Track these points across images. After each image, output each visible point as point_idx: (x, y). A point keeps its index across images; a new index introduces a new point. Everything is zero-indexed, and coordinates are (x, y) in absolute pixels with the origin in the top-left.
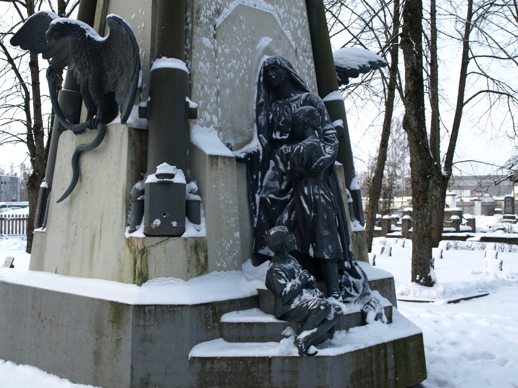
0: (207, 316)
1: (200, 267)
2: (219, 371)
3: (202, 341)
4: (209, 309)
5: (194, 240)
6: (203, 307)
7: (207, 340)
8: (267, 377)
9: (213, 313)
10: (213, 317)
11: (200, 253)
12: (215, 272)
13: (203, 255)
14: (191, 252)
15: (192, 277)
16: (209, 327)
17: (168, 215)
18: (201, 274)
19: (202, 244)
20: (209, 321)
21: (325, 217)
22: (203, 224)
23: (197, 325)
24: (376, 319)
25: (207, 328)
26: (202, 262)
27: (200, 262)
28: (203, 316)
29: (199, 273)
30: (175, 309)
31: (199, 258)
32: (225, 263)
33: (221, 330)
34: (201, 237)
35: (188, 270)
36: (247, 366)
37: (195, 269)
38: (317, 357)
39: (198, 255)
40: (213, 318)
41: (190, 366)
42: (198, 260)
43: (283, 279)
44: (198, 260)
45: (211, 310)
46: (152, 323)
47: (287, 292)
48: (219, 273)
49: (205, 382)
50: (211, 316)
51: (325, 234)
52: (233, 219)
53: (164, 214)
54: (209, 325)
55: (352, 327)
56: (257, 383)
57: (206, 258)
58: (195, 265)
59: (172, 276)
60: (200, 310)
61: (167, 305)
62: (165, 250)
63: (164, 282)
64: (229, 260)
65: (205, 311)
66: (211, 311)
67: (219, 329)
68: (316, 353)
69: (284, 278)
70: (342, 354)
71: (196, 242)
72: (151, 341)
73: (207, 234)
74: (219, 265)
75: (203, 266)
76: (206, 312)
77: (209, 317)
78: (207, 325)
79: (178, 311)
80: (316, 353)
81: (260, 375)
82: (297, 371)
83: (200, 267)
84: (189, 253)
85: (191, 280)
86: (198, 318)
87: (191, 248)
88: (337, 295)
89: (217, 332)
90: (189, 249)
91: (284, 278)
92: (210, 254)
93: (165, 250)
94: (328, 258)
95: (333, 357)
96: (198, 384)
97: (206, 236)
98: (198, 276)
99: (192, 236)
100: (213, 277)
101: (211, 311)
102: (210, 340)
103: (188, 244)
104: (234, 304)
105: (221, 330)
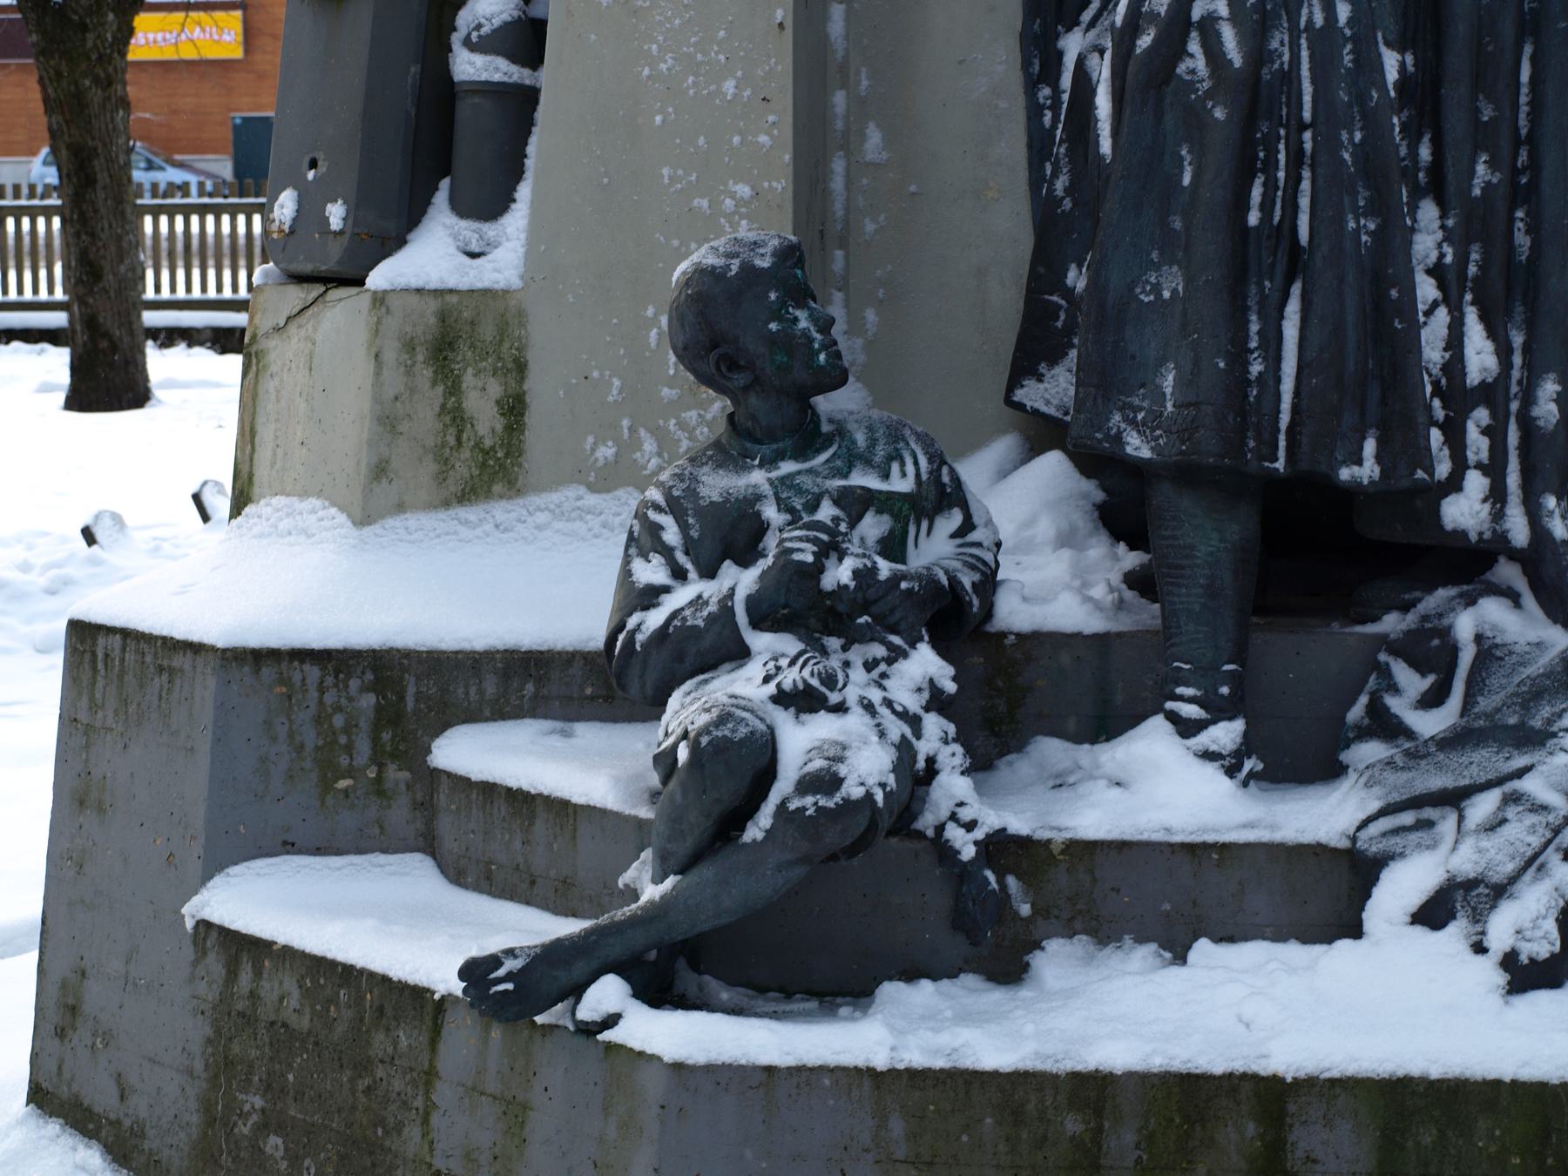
0: (338, 721)
1: (466, 453)
2: (273, 1017)
3: (289, 847)
4: (354, 684)
5: (432, 305)
6: (313, 672)
7: (318, 851)
8: (419, 1102)
9: (379, 709)
10: (376, 729)
11: (469, 380)
12: (570, 495)
13: (495, 389)
14: (409, 371)
15: (400, 508)
16: (343, 784)
17: (323, 166)
18: (469, 494)
19: (487, 332)
20: (349, 749)
21: (1187, 180)
22: (516, 221)
23: (263, 760)
24: (1432, 914)
25: (326, 786)
26: (483, 429)
27: (462, 426)
28: (304, 717)
29: (453, 487)
30: (179, 661)
31: (458, 408)
32: (649, 445)
33: (426, 808)
34: (486, 292)
35: (380, 471)
36: (362, 1020)
37: (431, 467)
38: (611, 1047)
39: (454, 389)
40: (375, 741)
41: (195, 963)
42: (455, 417)
43: (657, 559)
44: (455, 417)
45: (365, 689)
46: (110, 722)
47: (640, 638)
48: (592, 500)
49: (229, 1063)
50: (364, 724)
51: (1157, 289)
52: (744, 190)
53: (313, 164)
54: (349, 773)
55: (1219, 939)
56: (382, 1122)
57: (514, 409)
58: (430, 442)
59: (319, 494)
60: (283, 680)
61: (157, 637)
62: (311, 355)
63: (285, 524)
64: (682, 425)
65: (322, 690)
66: (368, 701)
67: (418, 806)
68: (612, 1021)
69: (667, 552)
70: (770, 1070)
71: (443, 317)
72: (101, 810)
73: (528, 277)
74: (606, 452)
75: (486, 453)
76: (329, 698)
77: (347, 730)
78: (328, 771)
79: (181, 670)
80: (612, 1021)
81: (397, 1085)
82: (525, 1107)
83: (466, 453)
84: (394, 381)
85: (395, 522)
86: (268, 723)
87: (409, 346)
88: (1191, 711)
89: (400, 813)
90: (390, 355)
91: (667, 552)
92: (542, 389)
93: (311, 355)
94: (1146, 453)
95: (678, 1067)
96: (207, 1066)
97: (516, 283)
98: (446, 504)
99: (415, 283)
100: (541, 518)
101: (368, 701)
102: (339, 852)
103: (392, 324)
104: (540, 681)
105: (426, 808)
